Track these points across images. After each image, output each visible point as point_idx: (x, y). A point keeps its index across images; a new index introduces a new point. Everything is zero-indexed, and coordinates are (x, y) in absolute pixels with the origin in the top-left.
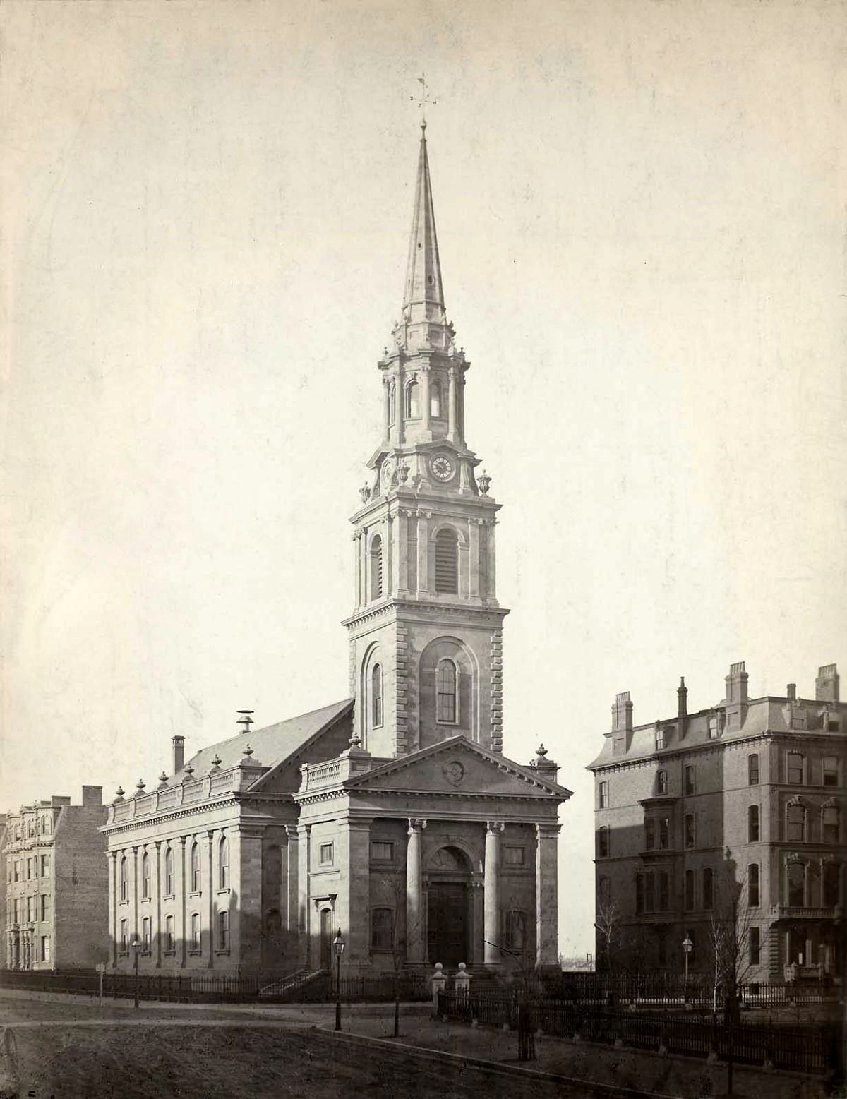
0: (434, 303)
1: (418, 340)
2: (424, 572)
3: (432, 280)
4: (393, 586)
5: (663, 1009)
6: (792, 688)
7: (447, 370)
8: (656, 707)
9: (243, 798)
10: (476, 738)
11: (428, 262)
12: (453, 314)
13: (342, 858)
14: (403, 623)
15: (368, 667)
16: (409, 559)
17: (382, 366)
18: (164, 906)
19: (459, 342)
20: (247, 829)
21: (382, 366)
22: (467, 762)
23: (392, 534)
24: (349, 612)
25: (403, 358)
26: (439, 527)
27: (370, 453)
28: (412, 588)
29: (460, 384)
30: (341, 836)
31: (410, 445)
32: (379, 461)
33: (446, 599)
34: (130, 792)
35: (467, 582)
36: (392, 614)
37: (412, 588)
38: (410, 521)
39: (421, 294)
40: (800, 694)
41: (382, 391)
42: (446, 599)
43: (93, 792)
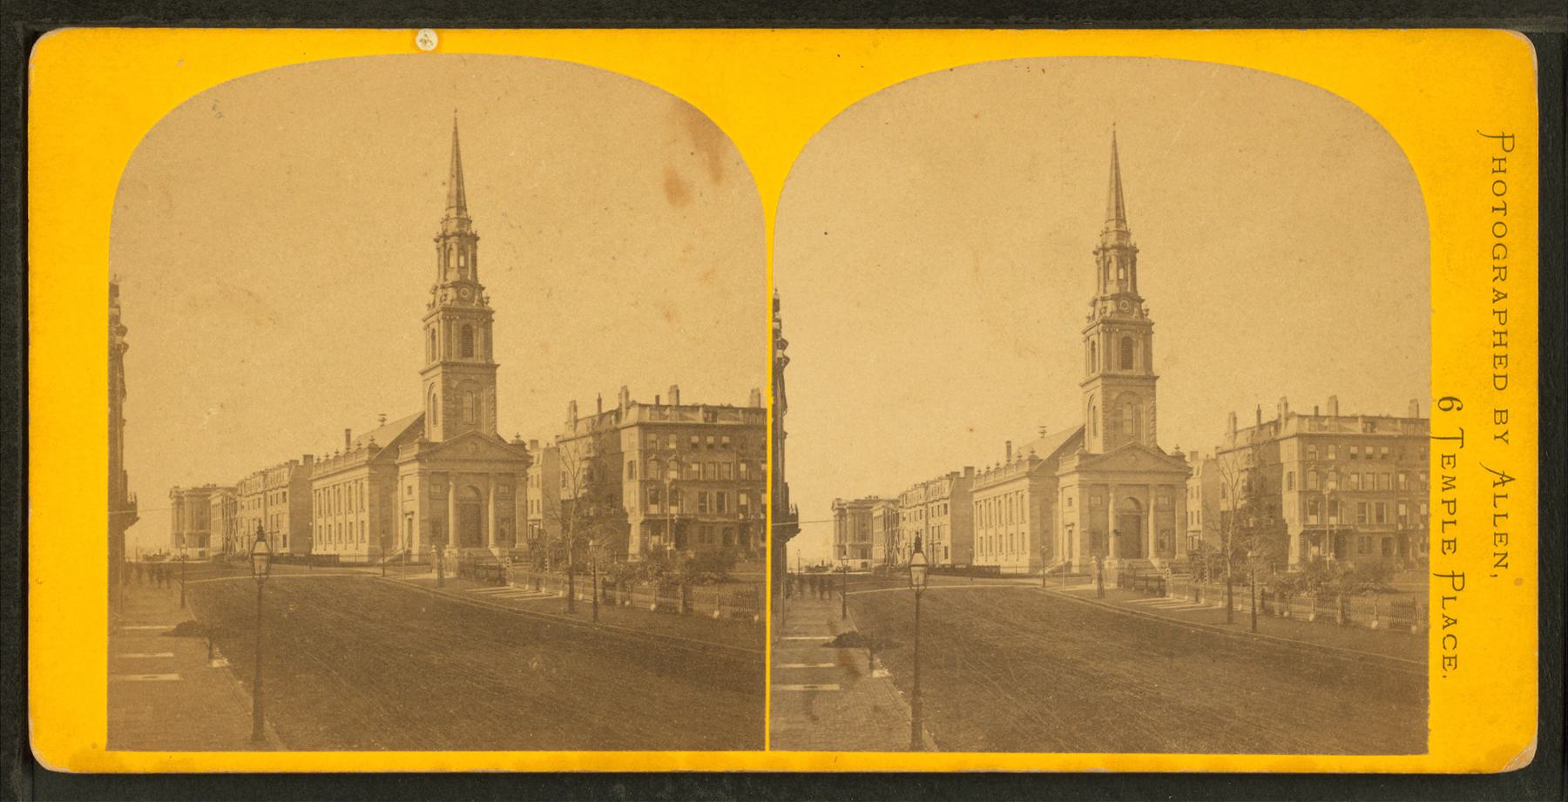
0: (1120, 219)
1: (1112, 240)
2: (455, 346)
3: (1119, 206)
4: (1101, 367)
5: (1094, 586)
6: (658, 398)
7: (1127, 256)
8: (588, 410)
9: (369, 463)
10: (484, 431)
11: (1117, 197)
12: (471, 212)
13: (1076, 502)
14: (1105, 386)
15: (430, 396)
16: (1108, 353)
17: (1096, 253)
18: (923, 526)
19: (1133, 240)
20: (372, 479)
21: (1096, 253)
22: (1138, 453)
23: (1099, 340)
24: (423, 367)
25: (1104, 249)
26: (465, 325)
27: (1090, 299)
28: (1109, 368)
29: (1134, 262)
30: (1074, 492)
31: (1108, 295)
32: (1094, 303)
33: (466, 361)
34: (323, 459)
35: (478, 350)
36: (440, 369)
37: (450, 355)
38: (1108, 333)
39: (454, 203)
40: (1321, 413)
41: (435, 253)
42: (1127, 373)
43: (308, 458)
